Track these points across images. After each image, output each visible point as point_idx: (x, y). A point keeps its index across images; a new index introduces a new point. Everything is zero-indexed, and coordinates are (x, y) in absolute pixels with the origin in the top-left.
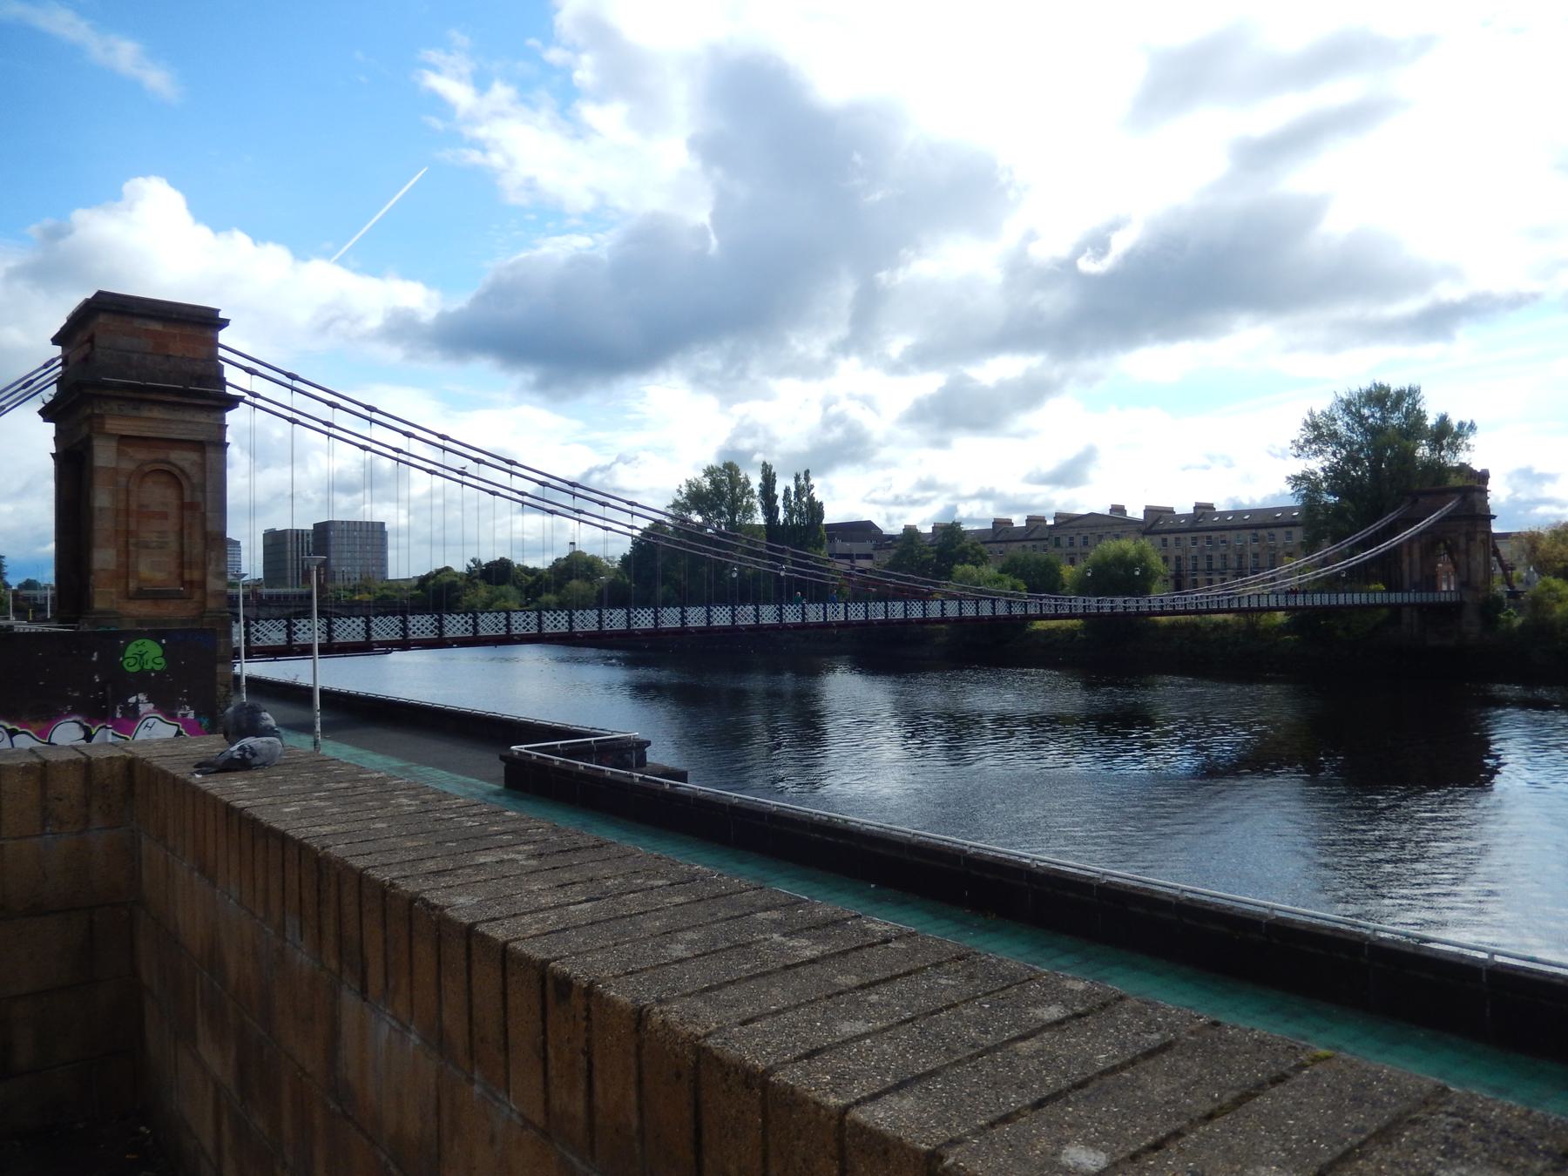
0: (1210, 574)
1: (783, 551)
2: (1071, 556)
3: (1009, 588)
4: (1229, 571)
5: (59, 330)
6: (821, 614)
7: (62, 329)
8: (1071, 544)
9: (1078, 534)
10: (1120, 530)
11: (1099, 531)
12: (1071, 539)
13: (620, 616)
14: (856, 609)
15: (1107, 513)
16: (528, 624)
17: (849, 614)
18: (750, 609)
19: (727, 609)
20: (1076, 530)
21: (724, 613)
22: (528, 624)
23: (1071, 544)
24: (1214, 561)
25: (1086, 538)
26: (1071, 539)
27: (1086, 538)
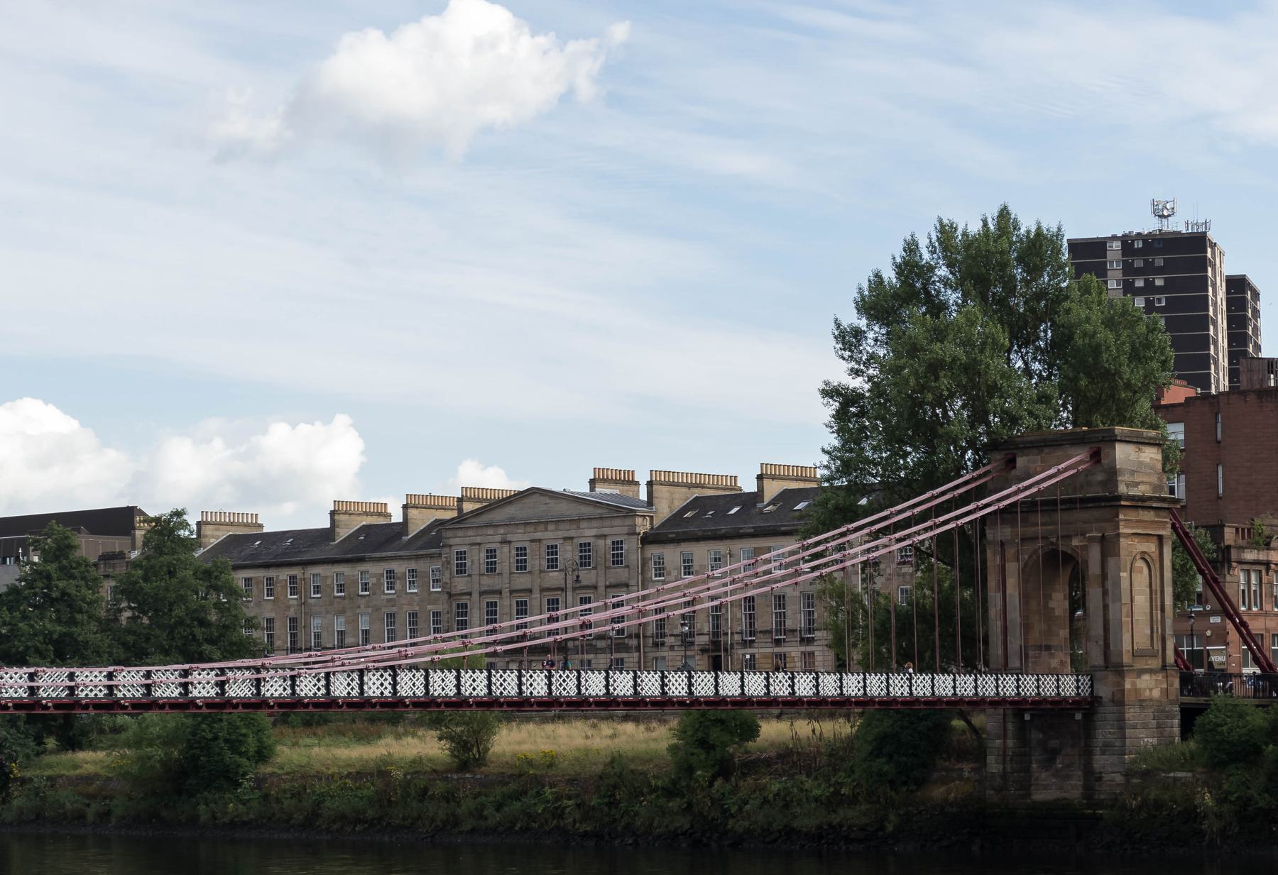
0: (778, 643)
1: (813, 569)
2: (491, 599)
3: (816, 653)
4: (818, 634)
5: (59, 411)
6: (355, 684)
7: (58, 408)
8: (491, 568)
9: (504, 542)
10: (594, 532)
11: (550, 535)
12: (491, 553)
13: (625, 681)
14: (382, 685)
15: (582, 488)
16: (474, 680)
17: (365, 687)
18: (949, 679)
19: (683, 676)
20: (502, 531)
21: (680, 680)
22: (474, 680)
23: (491, 568)
24: (758, 611)
25: (521, 551)
26: (585, 547)
27: (521, 551)
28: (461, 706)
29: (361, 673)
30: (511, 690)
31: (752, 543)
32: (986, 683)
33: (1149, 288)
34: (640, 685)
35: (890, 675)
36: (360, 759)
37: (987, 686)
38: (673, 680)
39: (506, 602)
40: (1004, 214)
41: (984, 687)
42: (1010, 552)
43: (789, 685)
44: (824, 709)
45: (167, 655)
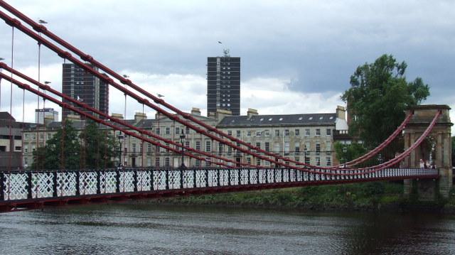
2: (198, 140)
12: (168, 129)
28: (139, 198)
29: (267, 169)
30: (91, 190)
31: (249, 129)
32: (88, 181)
33: (226, 97)
34: (58, 185)
35: (101, 173)
36: (314, 219)
37: (88, 183)
38: (109, 182)
39: (193, 141)
40: (452, 124)
41: (86, 184)
42: (412, 136)
43: (133, 182)
44: (143, 202)
45: (71, 167)
